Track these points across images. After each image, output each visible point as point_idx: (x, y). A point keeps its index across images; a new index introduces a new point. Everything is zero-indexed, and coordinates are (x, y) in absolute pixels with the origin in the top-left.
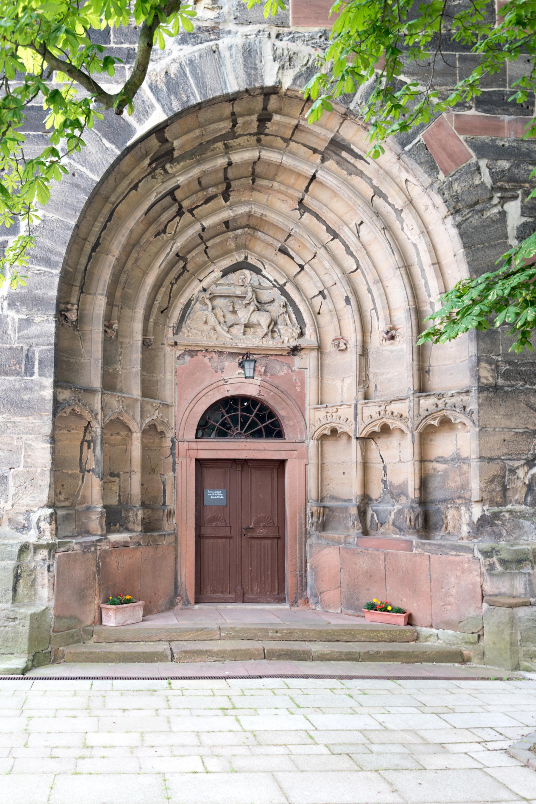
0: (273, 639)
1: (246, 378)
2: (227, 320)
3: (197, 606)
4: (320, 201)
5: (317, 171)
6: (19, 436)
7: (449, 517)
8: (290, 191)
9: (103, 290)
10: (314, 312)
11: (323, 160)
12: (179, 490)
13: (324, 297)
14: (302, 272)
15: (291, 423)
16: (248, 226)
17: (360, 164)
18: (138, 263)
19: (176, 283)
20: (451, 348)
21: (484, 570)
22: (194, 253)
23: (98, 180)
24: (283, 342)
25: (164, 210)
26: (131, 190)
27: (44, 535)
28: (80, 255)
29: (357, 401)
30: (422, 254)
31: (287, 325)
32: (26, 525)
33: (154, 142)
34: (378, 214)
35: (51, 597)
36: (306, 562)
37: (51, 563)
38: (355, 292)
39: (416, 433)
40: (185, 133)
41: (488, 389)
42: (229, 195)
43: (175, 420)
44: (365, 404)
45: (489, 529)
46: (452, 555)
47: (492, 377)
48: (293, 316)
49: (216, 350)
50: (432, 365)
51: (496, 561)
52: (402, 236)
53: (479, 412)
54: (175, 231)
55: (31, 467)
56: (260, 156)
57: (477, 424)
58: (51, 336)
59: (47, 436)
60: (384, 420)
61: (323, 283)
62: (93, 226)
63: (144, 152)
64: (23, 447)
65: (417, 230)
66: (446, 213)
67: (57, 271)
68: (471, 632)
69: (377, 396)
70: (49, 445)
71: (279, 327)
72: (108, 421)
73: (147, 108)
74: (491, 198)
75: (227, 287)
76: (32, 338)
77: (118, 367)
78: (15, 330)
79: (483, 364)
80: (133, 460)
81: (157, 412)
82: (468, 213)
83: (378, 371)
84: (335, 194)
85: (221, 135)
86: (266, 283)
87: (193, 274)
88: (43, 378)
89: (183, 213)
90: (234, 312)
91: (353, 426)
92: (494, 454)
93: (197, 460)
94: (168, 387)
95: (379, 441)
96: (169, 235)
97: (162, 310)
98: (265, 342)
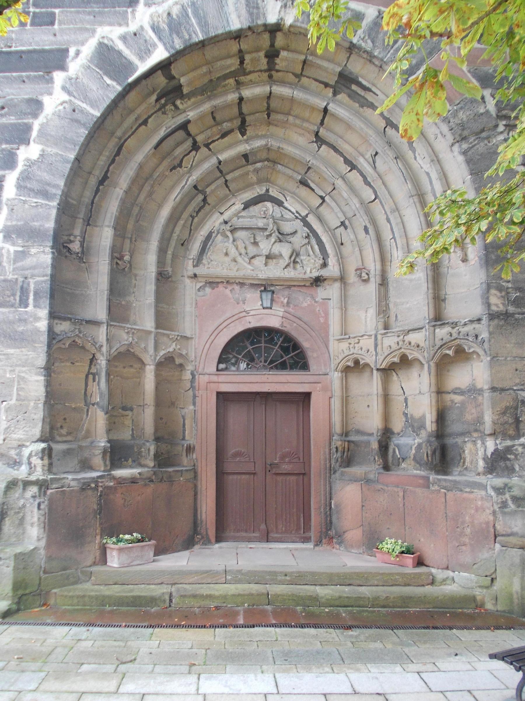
0: (282, 583)
1: (264, 308)
2: (248, 251)
3: (217, 545)
4: (335, 134)
5: (328, 104)
6: (12, 369)
7: (466, 452)
8: (305, 125)
9: (110, 222)
10: (337, 242)
11: (335, 94)
12: (199, 425)
13: (346, 228)
14: (324, 204)
15: (315, 355)
16: (268, 160)
17: (369, 97)
18: (154, 196)
19: (197, 215)
20: (465, 275)
21: (496, 507)
22: (213, 187)
23: (98, 114)
24: (305, 273)
25: (178, 145)
26: (140, 125)
27: (35, 470)
28: (84, 188)
29: (377, 332)
30: (434, 182)
31: (309, 256)
32: (18, 461)
33: (160, 80)
34: (390, 144)
35: (41, 536)
36: (331, 499)
37: (42, 500)
38: (374, 222)
39: (432, 364)
40: (193, 70)
41: (498, 317)
42: (246, 130)
43: (195, 352)
44: (385, 334)
45: (502, 464)
46: (466, 492)
47: (503, 304)
48: (316, 247)
49: (237, 281)
50: (448, 293)
51: (509, 498)
52: (415, 165)
53: (490, 341)
54: (192, 165)
55: (24, 400)
56: (271, 91)
57: (488, 352)
58: (47, 267)
59: (42, 368)
60: (403, 350)
61: (344, 213)
62: (98, 159)
63: (151, 89)
64: (16, 379)
65: (428, 160)
66: (452, 141)
67: (55, 203)
68: (485, 575)
69: (396, 327)
70: (43, 378)
71: (302, 258)
72: (116, 353)
73: (149, 46)
74: (497, 126)
75: (249, 219)
76: (27, 269)
77: (131, 298)
78: (10, 262)
79: (493, 291)
80: (146, 394)
81: (174, 344)
82: (475, 140)
83: (398, 301)
84: (349, 126)
85: (230, 72)
86: (288, 215)
87: (214, 207)
88: (38, 310)
89: (199, 148)
90: (255, 243)
91: (374, 357)
92: (507, 384)
93: (219, 394)
94: (187, 319)
95: (400, 373)
96: (185, 169)
97: (182, 242)
98: (286, 273)
